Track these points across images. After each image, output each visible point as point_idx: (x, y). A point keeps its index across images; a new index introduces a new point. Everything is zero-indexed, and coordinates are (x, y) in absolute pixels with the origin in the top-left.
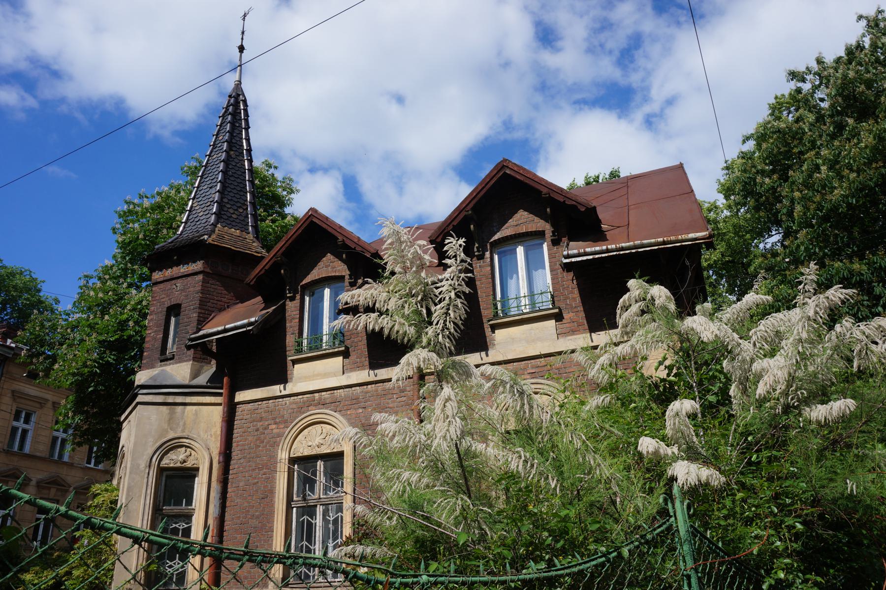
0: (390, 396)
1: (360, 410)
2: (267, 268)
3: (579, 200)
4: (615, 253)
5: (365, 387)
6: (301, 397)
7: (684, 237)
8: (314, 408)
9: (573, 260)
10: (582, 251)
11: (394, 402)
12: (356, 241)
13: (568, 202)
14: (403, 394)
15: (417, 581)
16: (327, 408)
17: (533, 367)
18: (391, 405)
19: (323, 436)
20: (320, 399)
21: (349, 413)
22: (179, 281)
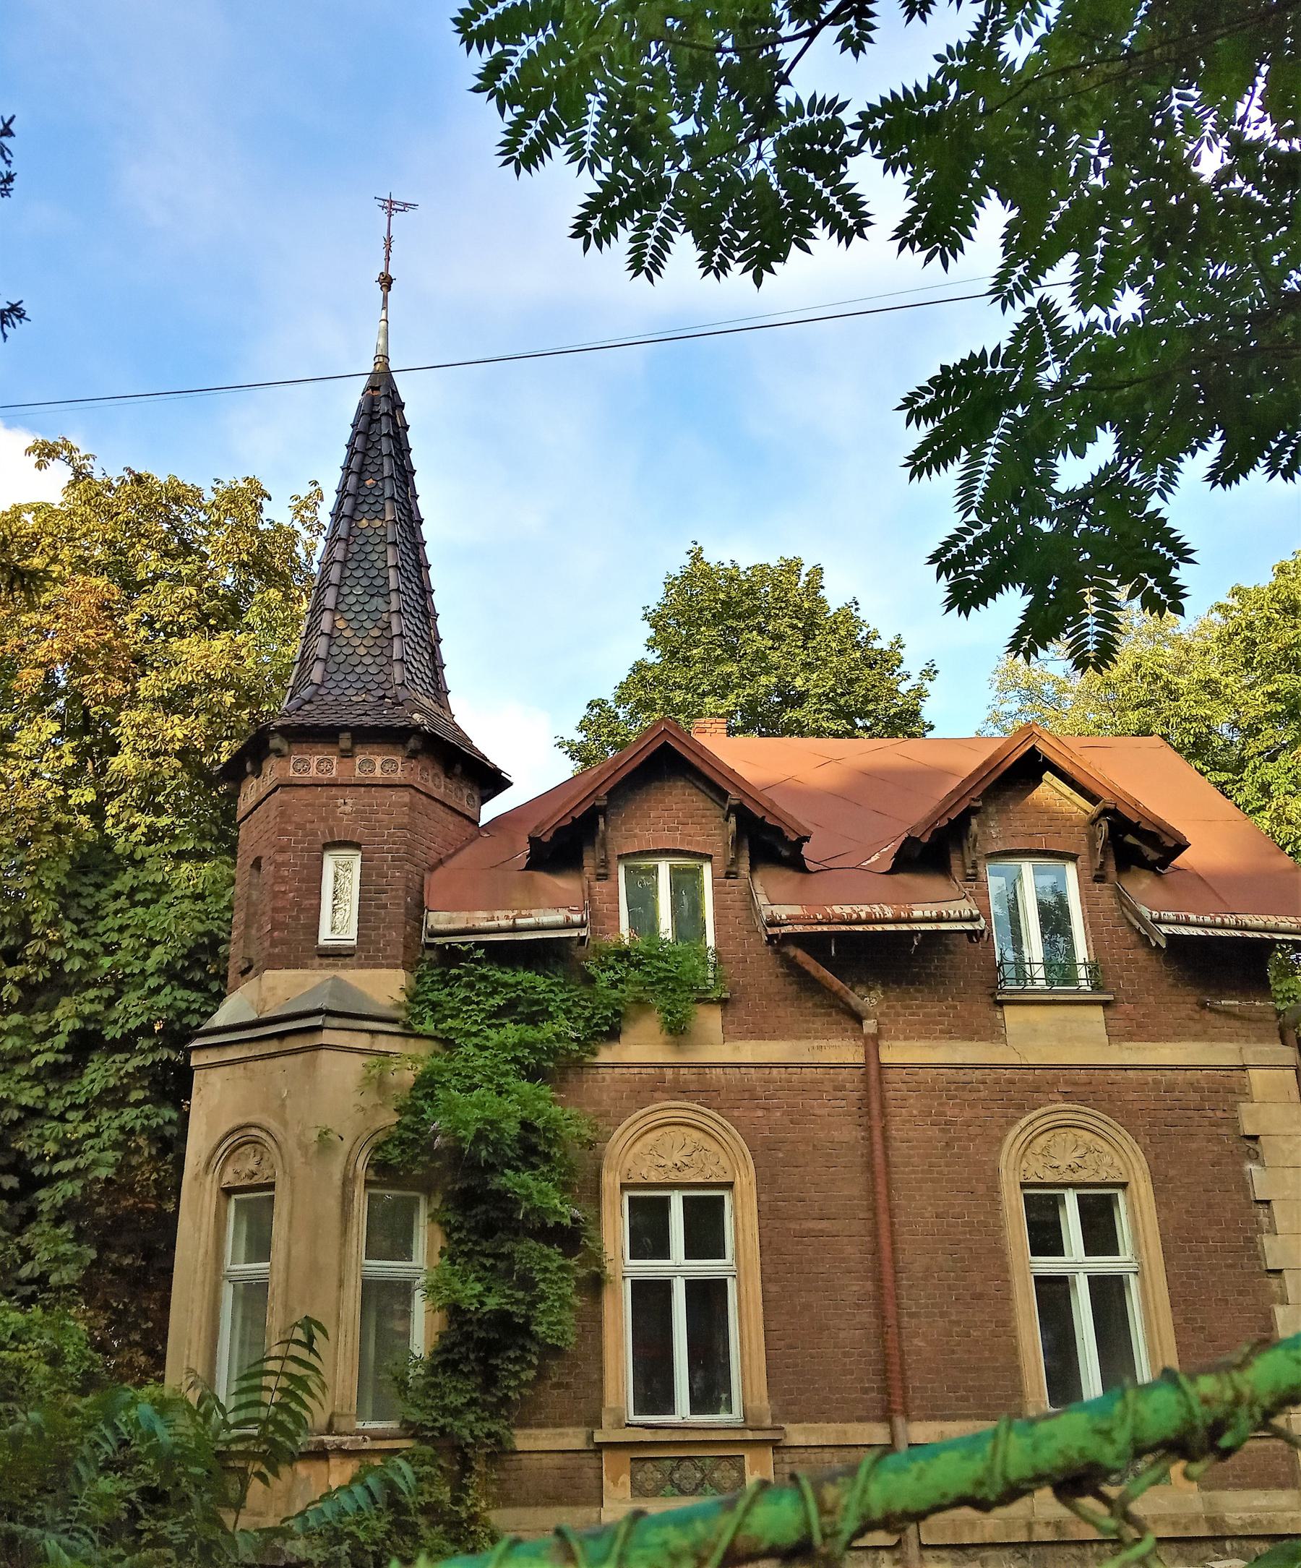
0: (816, 1095)
1: (760, 1113)
2: (577, 814)
3: (789, 822)
4: (1257, 935)
5: (767, 1071)
6: (636, 1070)
7: (1247, 919)
8: (666, 1096)
9: (1249, 935)
10: (1218, 920)
11: (820, 1106)
12: (766, 805)
13: (769, 820)
14: (840, 1094)
15: (70, 825)
16: (691, 1100)
17: (1066, 1082)
18: (817, 1112)
19: (687, 1151)
20: (676, 1080)
21: (736, 1114)
22: (827, 1450)
